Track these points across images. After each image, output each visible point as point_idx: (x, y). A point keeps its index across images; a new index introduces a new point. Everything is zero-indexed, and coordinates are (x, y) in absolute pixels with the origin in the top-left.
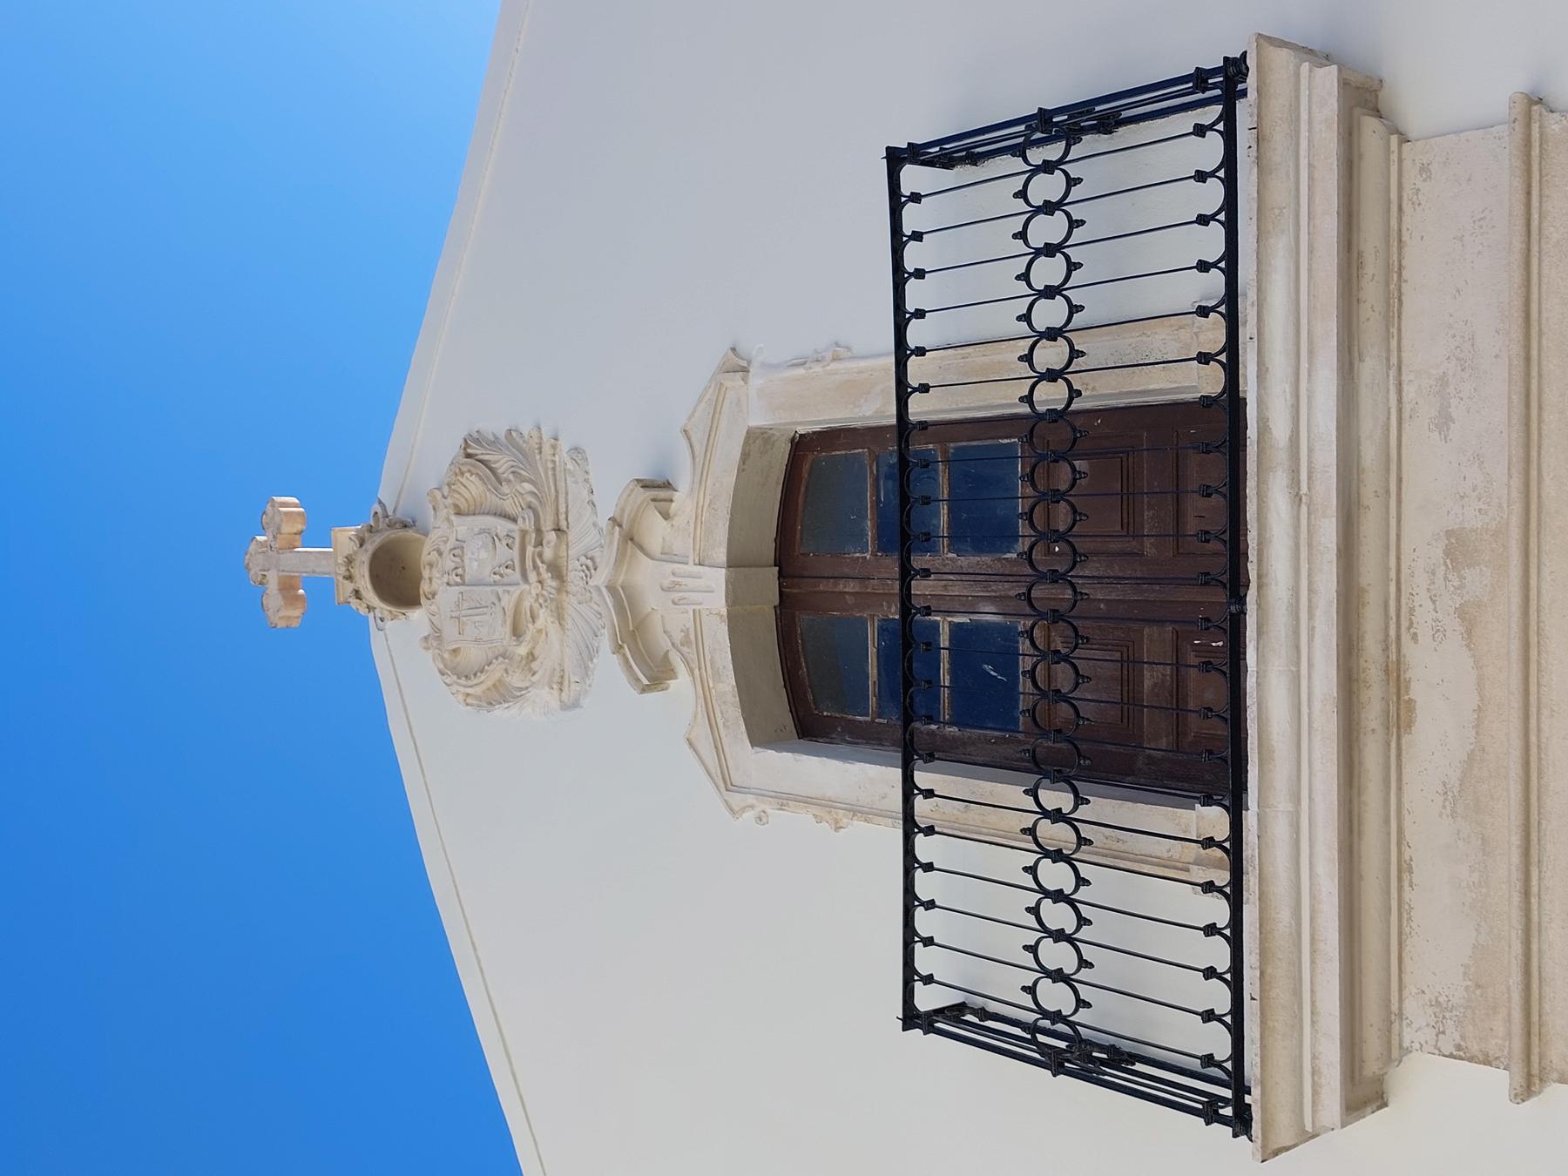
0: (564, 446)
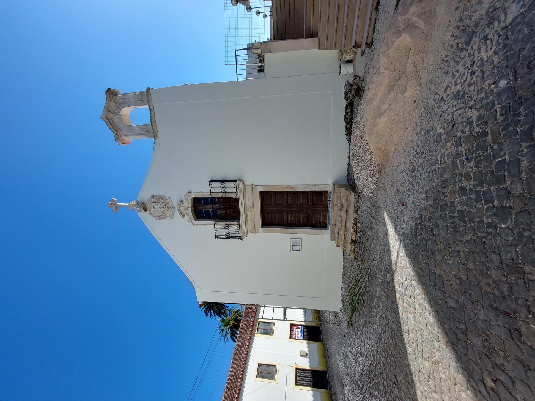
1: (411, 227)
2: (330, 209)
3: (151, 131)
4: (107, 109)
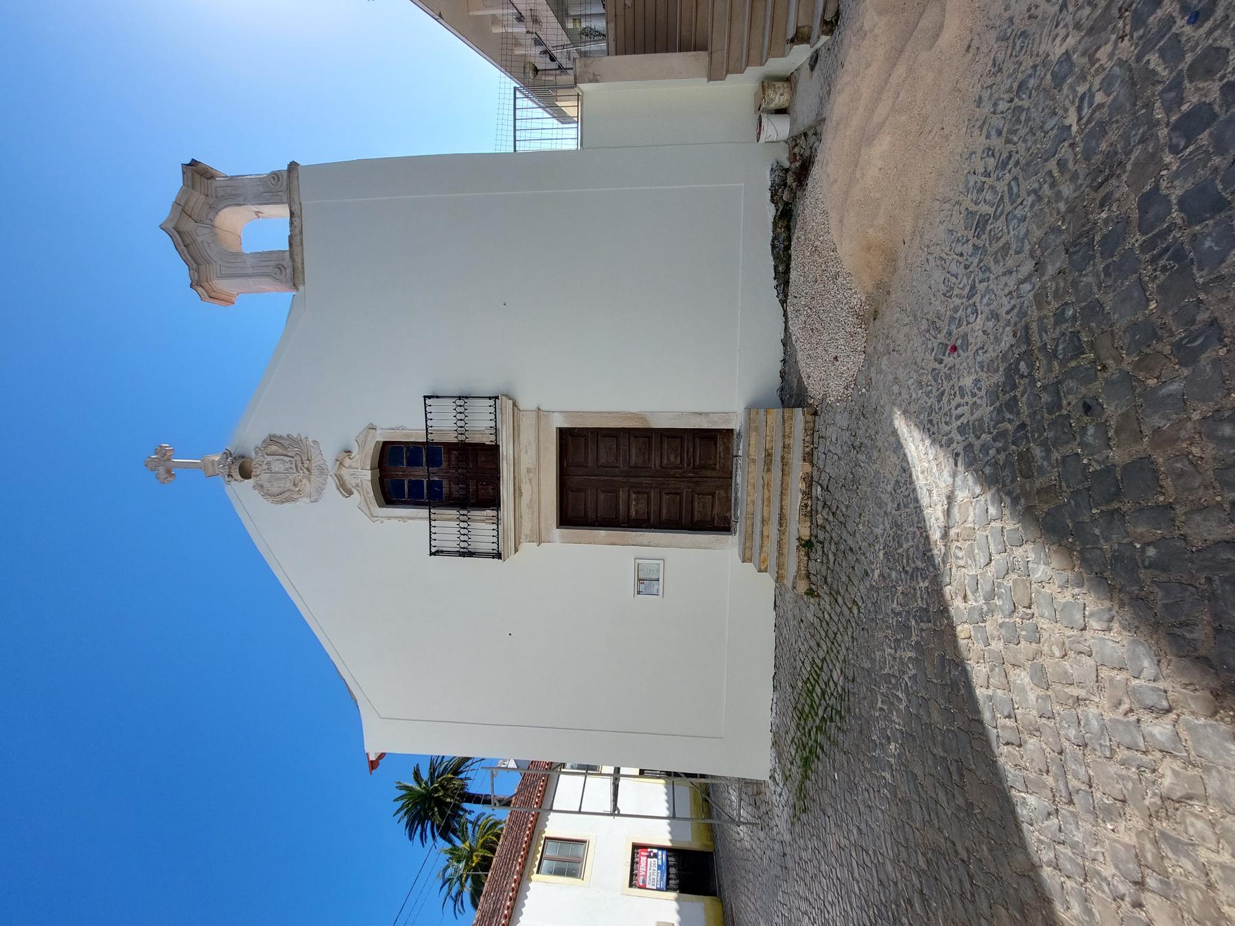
0: (310, 440)
1: (993, 395)
2: (739, 479)
3: (288, 268)
4: (182, 208)
